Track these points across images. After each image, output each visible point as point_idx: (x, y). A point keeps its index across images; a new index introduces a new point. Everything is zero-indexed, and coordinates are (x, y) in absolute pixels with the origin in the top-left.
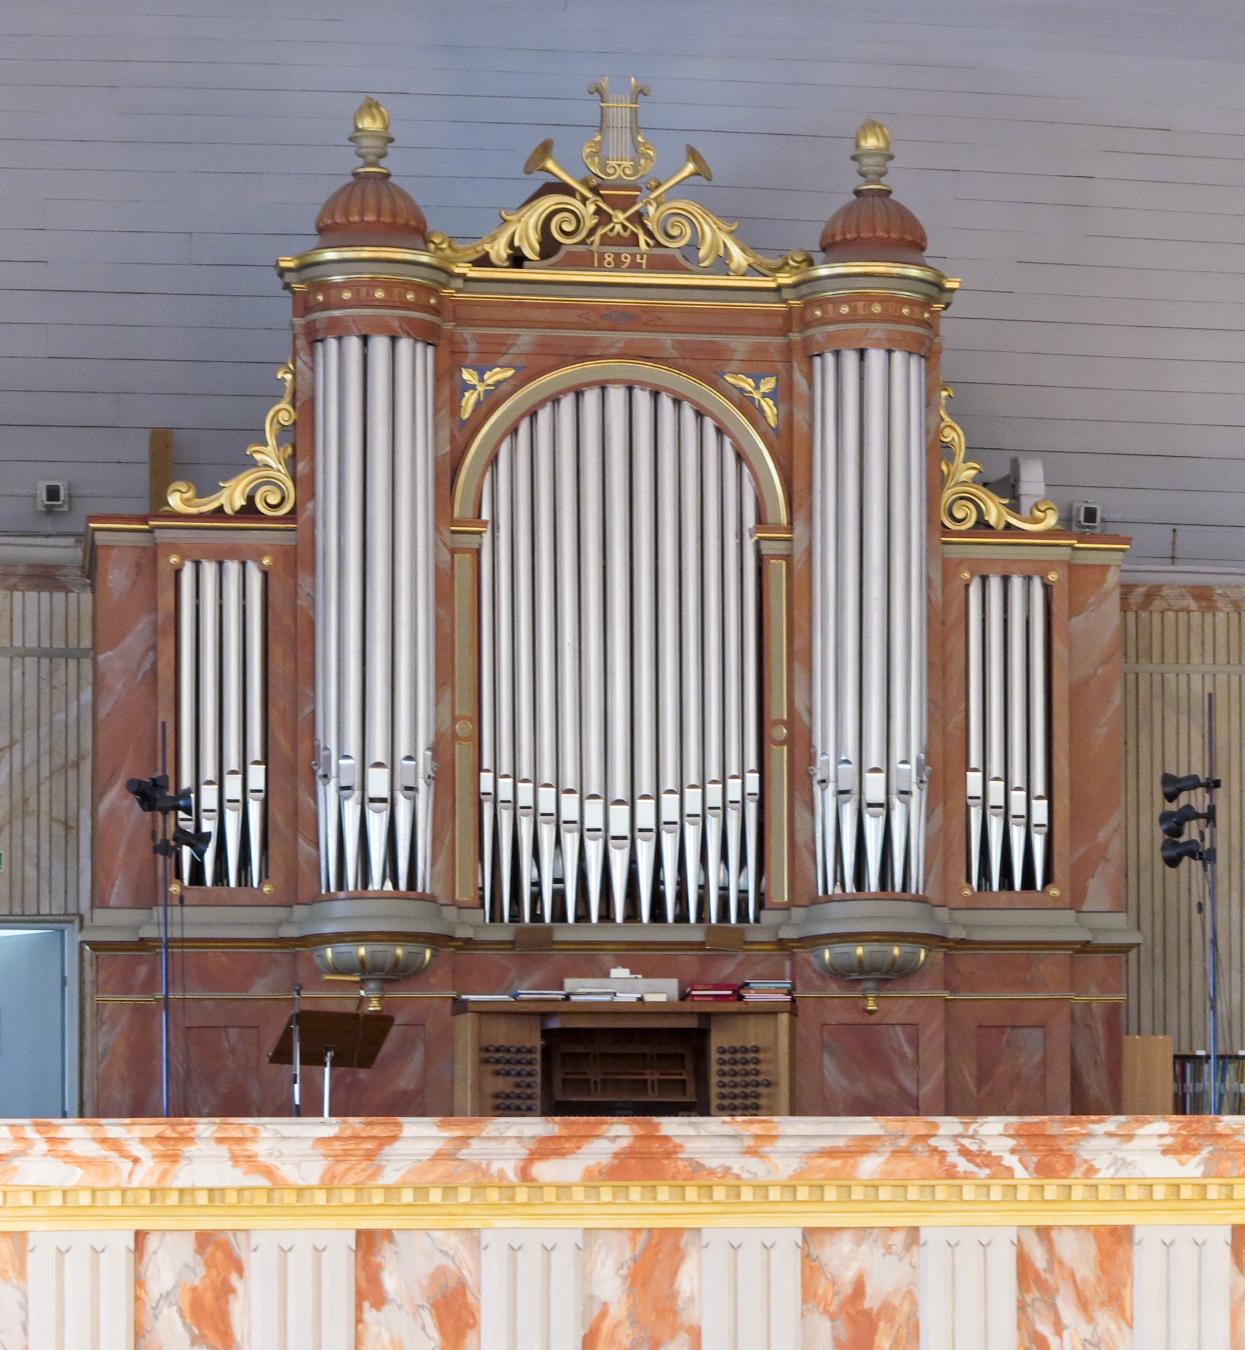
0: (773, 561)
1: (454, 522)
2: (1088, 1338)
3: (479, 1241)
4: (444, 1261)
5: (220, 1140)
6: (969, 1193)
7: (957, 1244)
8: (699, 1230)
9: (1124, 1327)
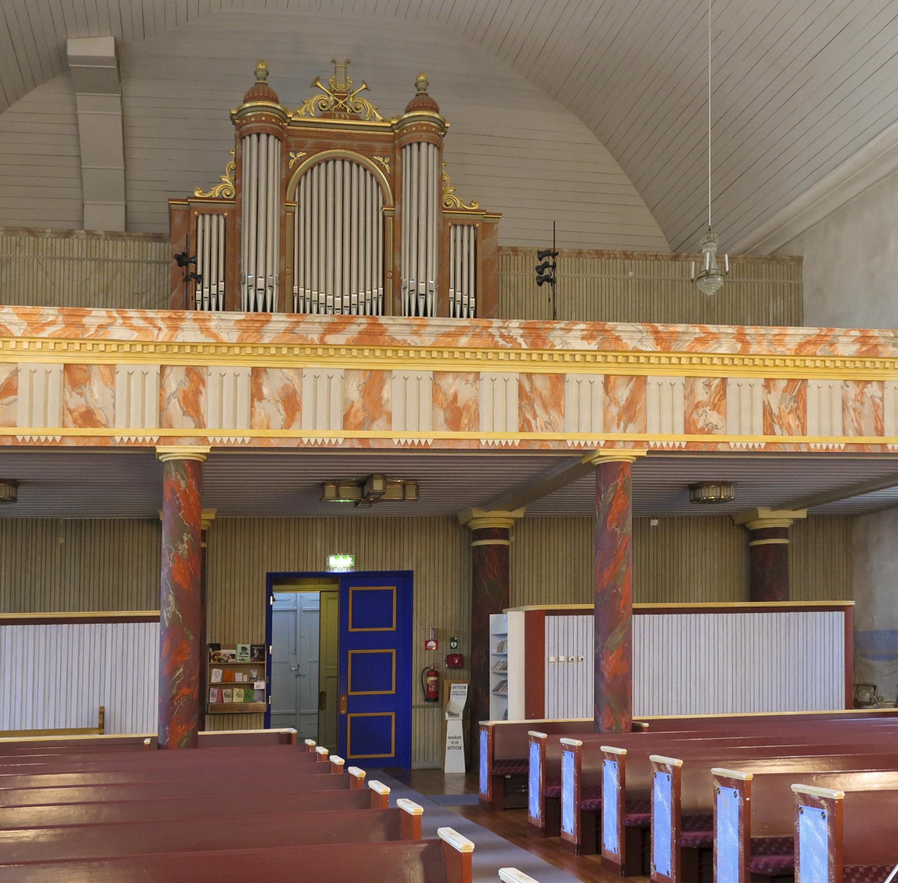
0: (388, 218)
2: (547, 420)
3: (302, 373)
4: (288, 382)
5: (195, 320)
6: (502, 356)
7: (495, 380)
8: (391, 371)
9: (561, 417)
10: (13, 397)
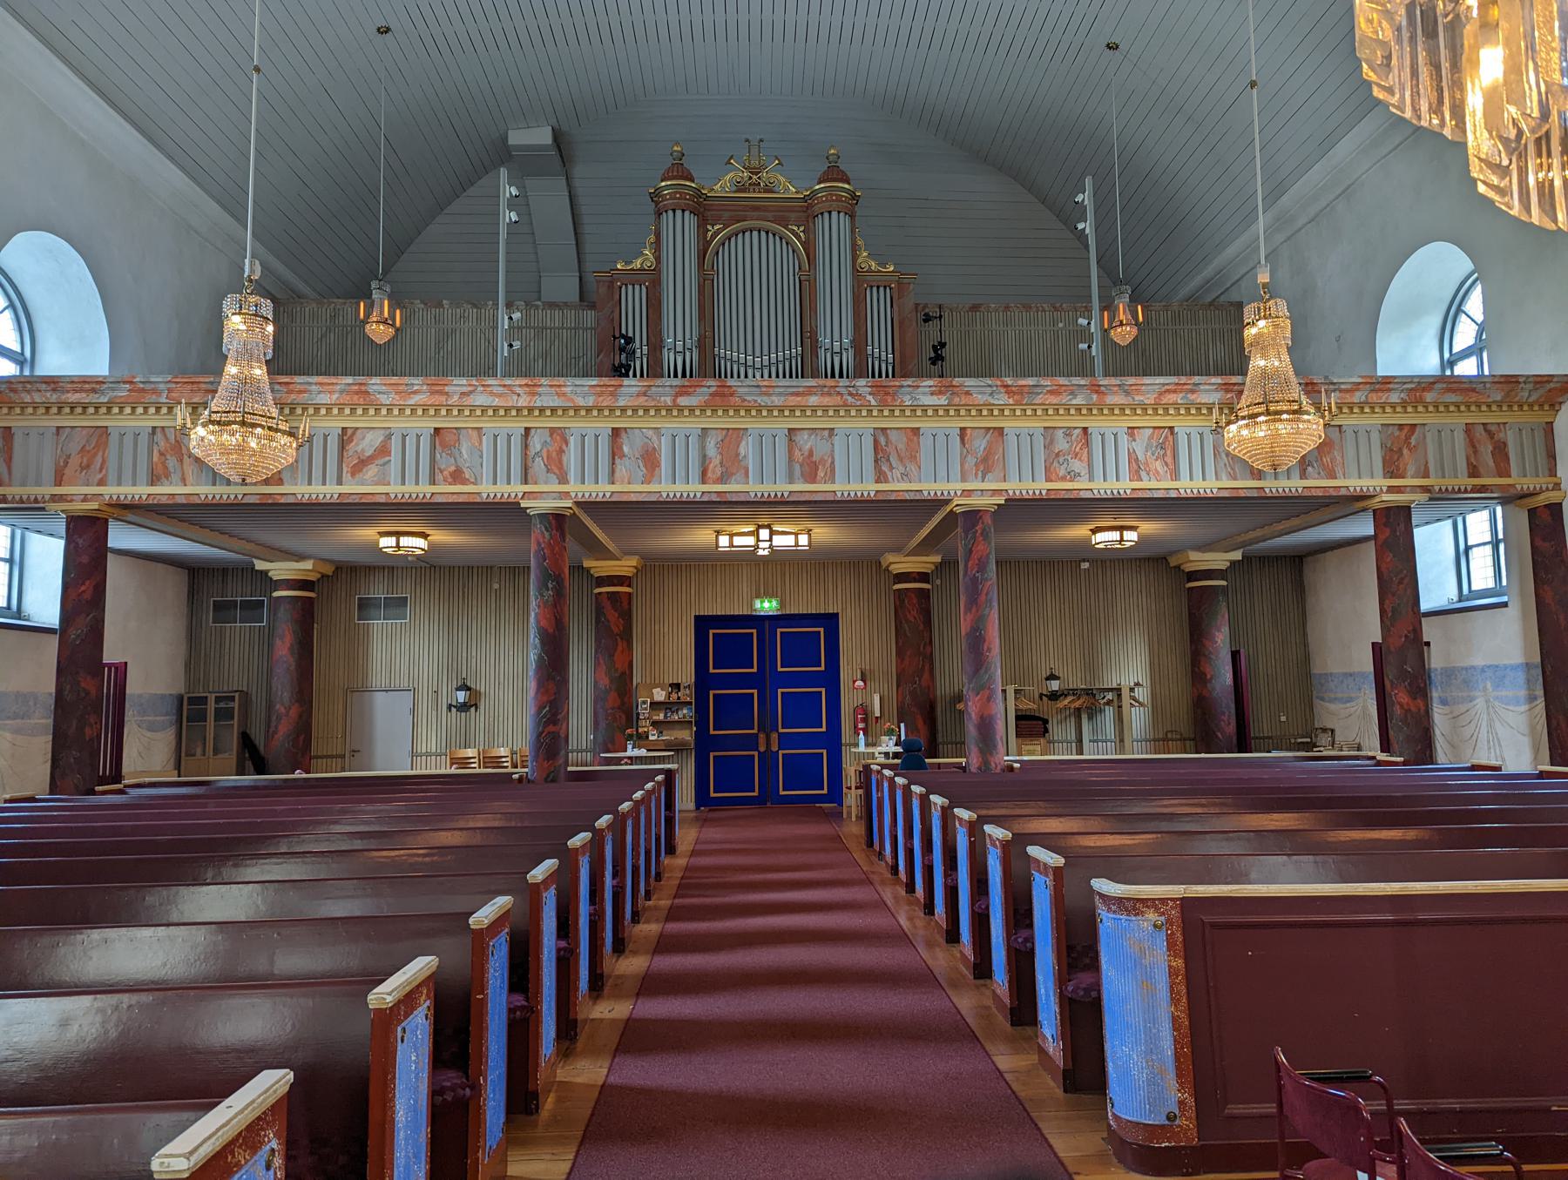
1: (704, 270)
8: (747, 429)
10: (387, 458)
